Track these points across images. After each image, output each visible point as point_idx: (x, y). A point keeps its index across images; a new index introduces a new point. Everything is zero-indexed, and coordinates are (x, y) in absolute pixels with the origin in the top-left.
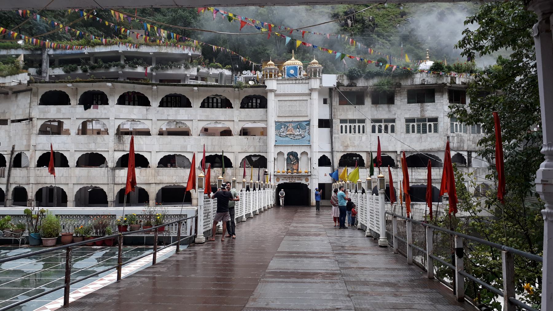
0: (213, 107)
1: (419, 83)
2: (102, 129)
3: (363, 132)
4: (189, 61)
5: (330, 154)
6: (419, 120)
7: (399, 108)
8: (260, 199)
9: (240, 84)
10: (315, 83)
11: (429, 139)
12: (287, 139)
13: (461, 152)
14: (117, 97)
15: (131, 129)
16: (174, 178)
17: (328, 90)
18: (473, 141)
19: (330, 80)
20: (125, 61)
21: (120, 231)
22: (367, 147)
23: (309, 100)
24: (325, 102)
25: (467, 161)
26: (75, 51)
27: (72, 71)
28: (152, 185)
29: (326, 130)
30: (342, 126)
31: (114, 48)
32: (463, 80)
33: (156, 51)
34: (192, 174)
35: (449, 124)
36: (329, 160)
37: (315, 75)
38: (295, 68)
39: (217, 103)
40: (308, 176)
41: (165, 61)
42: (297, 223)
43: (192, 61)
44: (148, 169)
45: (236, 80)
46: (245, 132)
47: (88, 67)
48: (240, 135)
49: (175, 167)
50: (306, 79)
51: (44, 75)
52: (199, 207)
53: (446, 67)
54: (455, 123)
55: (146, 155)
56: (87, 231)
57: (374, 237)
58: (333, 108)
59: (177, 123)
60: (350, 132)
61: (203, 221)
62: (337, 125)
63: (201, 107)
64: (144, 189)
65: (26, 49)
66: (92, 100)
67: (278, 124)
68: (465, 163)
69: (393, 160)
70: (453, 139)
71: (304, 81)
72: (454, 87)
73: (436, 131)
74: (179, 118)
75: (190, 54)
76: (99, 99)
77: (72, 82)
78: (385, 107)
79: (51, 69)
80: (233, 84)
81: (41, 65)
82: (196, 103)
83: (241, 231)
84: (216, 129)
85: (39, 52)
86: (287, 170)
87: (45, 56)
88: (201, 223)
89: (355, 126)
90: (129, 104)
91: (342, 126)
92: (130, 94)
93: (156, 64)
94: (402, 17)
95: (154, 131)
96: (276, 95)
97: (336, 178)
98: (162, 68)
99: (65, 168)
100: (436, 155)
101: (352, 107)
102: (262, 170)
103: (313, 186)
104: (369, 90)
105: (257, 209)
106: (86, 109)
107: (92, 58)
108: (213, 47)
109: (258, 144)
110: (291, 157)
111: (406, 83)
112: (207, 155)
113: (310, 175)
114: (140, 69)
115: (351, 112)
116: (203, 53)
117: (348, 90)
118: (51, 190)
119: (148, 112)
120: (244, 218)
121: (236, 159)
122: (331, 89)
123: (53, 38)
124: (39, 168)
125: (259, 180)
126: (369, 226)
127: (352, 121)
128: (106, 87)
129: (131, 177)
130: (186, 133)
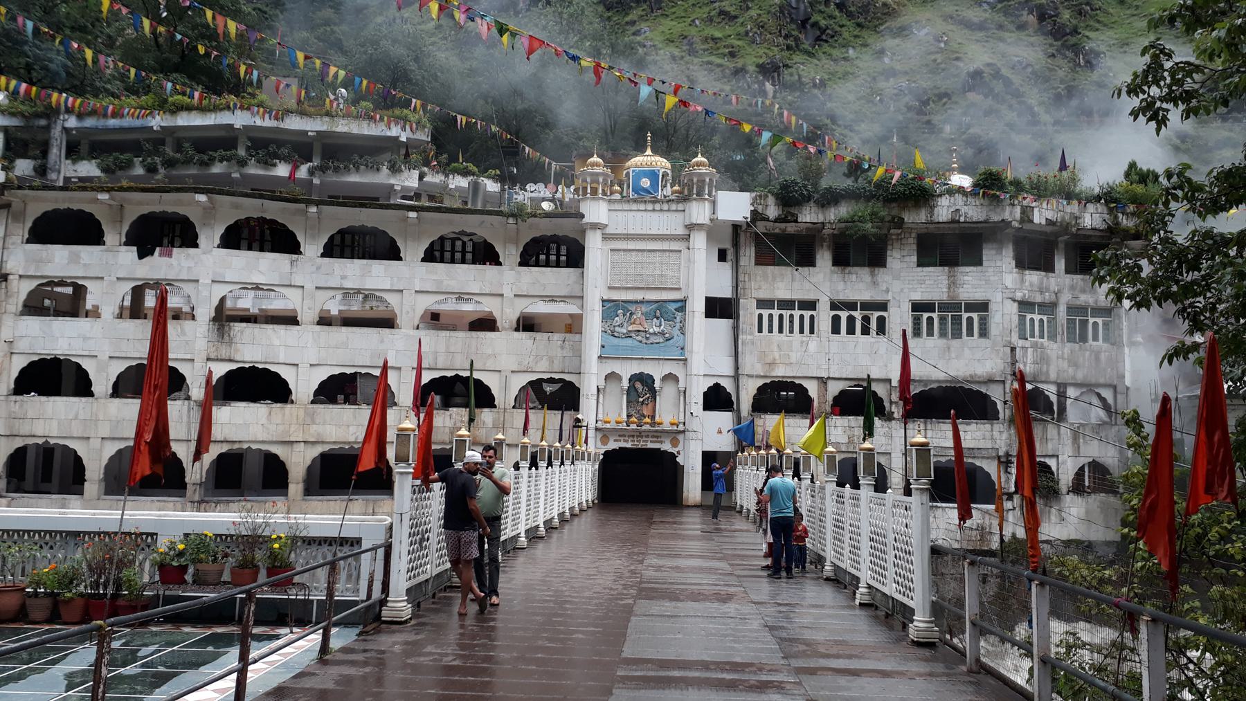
0: (453, 261)
2: (186, 309)
3: (812, 332)
5: (731, 380)
6: (944, 307)
7: (897, 278)
8: (562, 488)
9: (521, 207)
10: (699, 212)
11: (967, 351)
12: (629, 341)
13: (1041, 386)
15: (254, 311)
17: (730, 230)
18: (1069, 361)
19: (735, 206)
20: (248, 149)
21: (164, 581)
22: (819, 367)
24: (722, 256)
25: (1055, 408)
26: (127, 122)
27: (121, 168)
28: (295, 445)
29: (724, 324)
30: (760, 316)
31: (224, 118)
32: (1050, 215)
33: (324, 128)
34: (377, 422)
35: (1015, 319)
38: (653, 175)
39: (464, 252)
40: (676, 434)
41: (337, 152)
42: (660, 556)
43: (407, 155)
44: (289, 406)
45: (510, 198)
46: (527, 324)
47: (157, 160)
48: (517, 330)
49: (355, 403)
50: (678, 202)
51: (53, 176)
52: (396, 518)
53: (1011, 183)
54: (1029, 316)
55: (285, 373)
56: (69, 580)
57: (889, 614)
58: (740, 270)
59: (366, 297)
60: (781, 331)
61: (405, 558)
62: (749, 313)
63: (423, 260)
64: (276, 457)
65: (13, 114)
66: (154, 234)
68: (1051, 412)
70: (1025, 355)
71: (674, 207)
73: (984, 333)
74: (370, 284)
75: (403, 139)
76: (178, 233)
77: (109, 190)
78: (864, 272)
79: (69, 162)
80: (504, 208)
81: (45, 153)
82: (413, 251)
83: (516, 579)
84: (460, 315)
85: (43, 122)
86: (629, 416)
87: (56, 132)
88: (400, 564)
89: (791, 316)
90: (250, 249)
91: (760, 316)
93: (322, 159)
95: (307, 314)
96: (606, 237)
97: (745, 437)
98: (336, 170)
99: (84, 399)
100: (983, 390)
101: (788, 271)
102: (569, 416)
105: (555, 513)
106: (141, 256)
107: (169, 140)
108: (459, 117)
109: (559, 353)
110: (638, 385)
111: (916, 217)
113: (684, 432)
114: (282, 170)
115: (785, 282)
116: (435, 138)
117: (777, 231)
118: (48, 452)
119: (294, 270)
120: (523, 540)
121: (505, 388)
122: (736, 227)
123: (77, 89)
124: (19, 398)
125: (560, 440)
126: (865, 576)
127: (787, 304)
128: (193, 205)
129: (152, 424)
130: (387, 322)
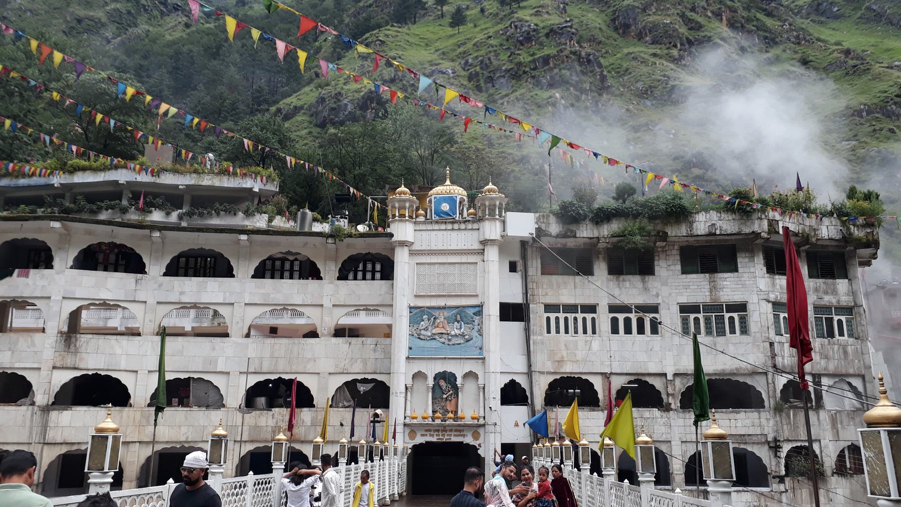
1: (703, 233)
3: (594, 332)
4: (259, 202)
6: (708, 308)
7: (665, 284)
10: (491, 230)
12: (433, 343)
14: (73, 254)
16: (184, 429)
17: (518, 245)
20: (129, 200)
22: (602, 363)
23: (480, 264)
24: (513, 268)
25: (813, 396)
29: (516, 327)
30: (548, 319)
33: (192, 182)
35: (771, 317)
36: (524, 390)
37: (492, 214)
38: (451, 200)
40: (477, 428)
44: (126, 409)
49: (187, 406)
50: (473, 222)
58: (529, 279)
60: (567, 332)
63: (253, 277)
67: (414, 311)
69: (659, 392)
70: (782, 349)
71: (470, 226)
72: (774, 242)
73: (745, 330)
74: (205, 298)
75: (256, 190)
78: (636, 280)
82: (244, 269)
86: (434, 412)
91: (548, 319)
92: (104, 248)
93: (192, 205)
96: (412, 253)
97: (539, 429)
98: (201, 215)
100: (749, 381)
103: (489, 448)
104: (601, 245)
107: (68, 195)
108: (288, 158)
109: (372, 355)
110: (442, 383)
111: (678, 232)
112: (169, 377)
113: (484, 425)
115: (569, 290)
119: (139, 287)
121: (323, 389)
122: (524, 243)
127: (571, 308)
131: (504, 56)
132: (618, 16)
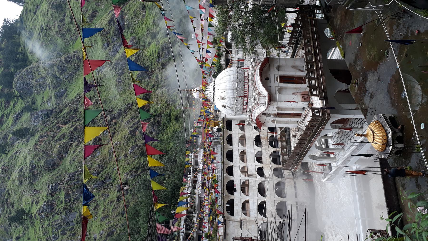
49: (261, 158)
94: (128, 156)
131: (57, 217)
132: (48, 168)
